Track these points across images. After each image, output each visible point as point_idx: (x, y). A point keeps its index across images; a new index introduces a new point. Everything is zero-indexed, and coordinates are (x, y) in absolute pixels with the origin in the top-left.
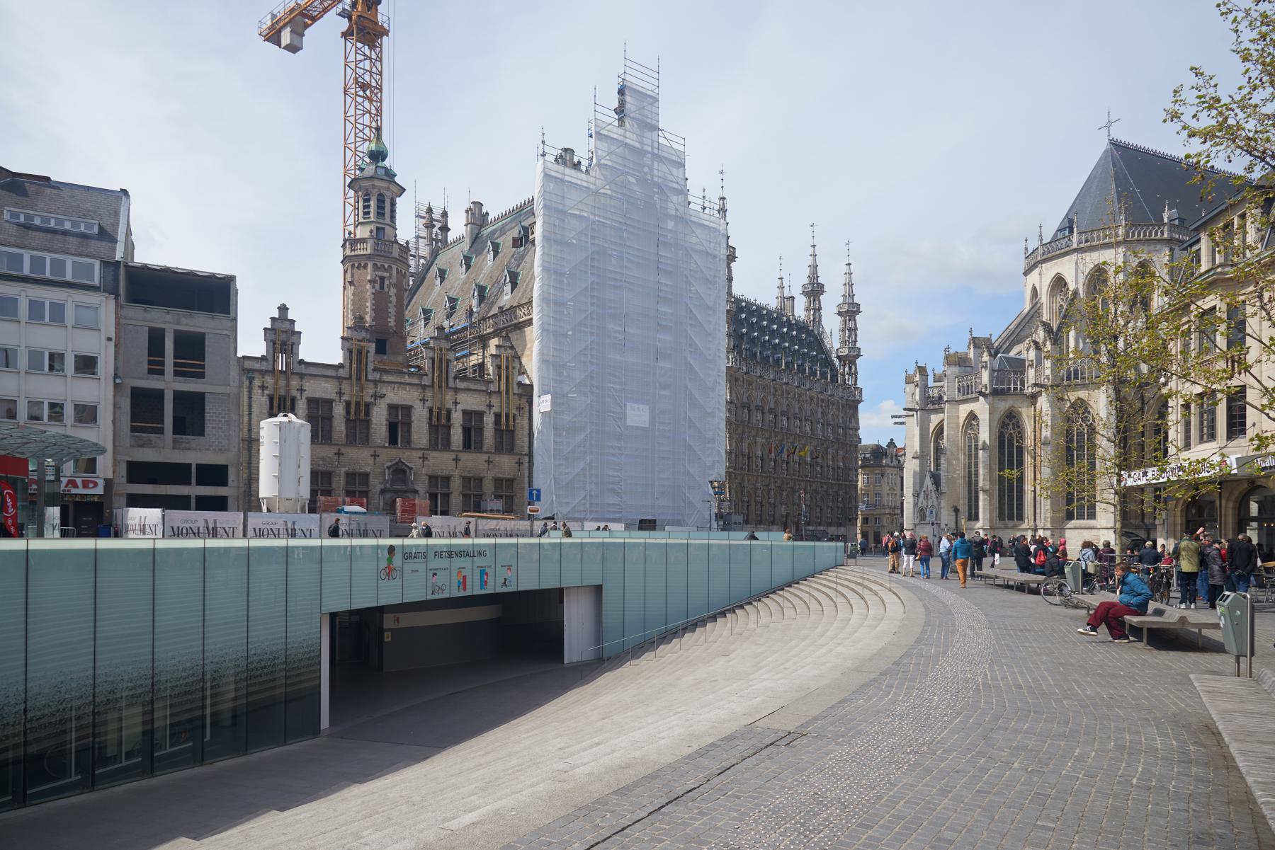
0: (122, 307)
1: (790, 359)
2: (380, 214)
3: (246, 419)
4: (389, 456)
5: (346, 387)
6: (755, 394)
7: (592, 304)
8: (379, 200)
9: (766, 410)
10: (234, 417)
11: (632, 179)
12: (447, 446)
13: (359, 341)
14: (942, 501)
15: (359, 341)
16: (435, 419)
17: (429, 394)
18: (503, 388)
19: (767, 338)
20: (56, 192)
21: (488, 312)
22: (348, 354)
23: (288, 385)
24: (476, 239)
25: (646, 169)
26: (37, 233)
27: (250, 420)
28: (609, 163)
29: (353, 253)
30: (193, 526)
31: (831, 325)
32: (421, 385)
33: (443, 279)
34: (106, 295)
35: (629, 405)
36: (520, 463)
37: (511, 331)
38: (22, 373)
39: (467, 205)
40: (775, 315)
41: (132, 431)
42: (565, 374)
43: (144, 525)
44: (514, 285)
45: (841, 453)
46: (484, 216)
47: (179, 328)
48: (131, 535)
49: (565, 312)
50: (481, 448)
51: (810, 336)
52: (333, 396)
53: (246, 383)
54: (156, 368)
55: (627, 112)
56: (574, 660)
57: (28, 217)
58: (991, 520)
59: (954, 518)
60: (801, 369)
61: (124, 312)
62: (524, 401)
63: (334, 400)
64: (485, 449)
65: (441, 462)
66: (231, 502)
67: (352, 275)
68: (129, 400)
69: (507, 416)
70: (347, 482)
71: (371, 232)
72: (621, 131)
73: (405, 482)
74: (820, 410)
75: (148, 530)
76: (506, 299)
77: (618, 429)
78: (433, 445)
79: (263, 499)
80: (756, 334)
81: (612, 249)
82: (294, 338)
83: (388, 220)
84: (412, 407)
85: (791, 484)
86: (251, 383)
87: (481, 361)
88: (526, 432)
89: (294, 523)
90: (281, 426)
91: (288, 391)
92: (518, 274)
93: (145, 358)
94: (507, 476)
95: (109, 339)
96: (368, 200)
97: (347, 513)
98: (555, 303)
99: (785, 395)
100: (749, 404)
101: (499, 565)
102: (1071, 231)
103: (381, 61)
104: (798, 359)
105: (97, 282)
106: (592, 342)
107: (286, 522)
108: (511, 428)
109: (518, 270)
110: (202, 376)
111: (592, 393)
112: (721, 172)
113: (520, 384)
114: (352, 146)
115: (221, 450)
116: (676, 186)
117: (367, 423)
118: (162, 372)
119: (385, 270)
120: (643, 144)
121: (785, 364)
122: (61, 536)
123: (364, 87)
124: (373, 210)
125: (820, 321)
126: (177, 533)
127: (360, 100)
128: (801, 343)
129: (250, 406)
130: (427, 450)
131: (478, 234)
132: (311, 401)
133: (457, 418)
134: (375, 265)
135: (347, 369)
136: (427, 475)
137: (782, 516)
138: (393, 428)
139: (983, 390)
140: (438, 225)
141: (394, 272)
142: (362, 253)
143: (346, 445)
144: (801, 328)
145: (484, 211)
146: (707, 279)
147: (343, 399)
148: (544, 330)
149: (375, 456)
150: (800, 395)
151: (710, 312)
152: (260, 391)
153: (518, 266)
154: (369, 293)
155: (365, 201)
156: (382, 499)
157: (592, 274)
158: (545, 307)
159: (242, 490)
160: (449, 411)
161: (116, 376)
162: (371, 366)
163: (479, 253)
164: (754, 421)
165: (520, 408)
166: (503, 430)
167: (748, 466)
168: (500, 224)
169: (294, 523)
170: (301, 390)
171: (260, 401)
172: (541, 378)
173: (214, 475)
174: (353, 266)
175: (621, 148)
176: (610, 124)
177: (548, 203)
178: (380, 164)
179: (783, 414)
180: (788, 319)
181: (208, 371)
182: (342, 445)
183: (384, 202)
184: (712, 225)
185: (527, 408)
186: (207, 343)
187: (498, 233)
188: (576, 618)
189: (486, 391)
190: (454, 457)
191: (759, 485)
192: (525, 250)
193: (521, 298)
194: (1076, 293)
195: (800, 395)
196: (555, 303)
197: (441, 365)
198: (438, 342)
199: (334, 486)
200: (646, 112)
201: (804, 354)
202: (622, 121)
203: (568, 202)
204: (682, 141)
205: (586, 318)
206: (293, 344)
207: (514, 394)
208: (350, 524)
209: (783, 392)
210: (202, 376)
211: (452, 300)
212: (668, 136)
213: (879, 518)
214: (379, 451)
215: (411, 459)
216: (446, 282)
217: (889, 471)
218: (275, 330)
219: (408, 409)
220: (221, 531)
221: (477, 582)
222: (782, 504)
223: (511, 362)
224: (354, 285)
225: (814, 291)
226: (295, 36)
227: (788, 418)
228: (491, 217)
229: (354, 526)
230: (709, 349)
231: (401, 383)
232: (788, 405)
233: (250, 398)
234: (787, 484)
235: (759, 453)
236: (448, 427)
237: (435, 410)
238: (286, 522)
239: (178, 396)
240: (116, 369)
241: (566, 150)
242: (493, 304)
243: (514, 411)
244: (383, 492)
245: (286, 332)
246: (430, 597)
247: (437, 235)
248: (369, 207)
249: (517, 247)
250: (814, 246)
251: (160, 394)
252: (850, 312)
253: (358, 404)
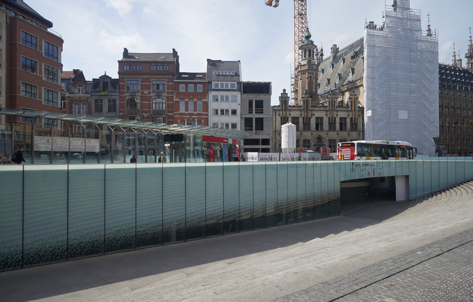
0: (242, 95)
1: (461, 85)
2: (310, 56)
3: (275, 125)
4: (316, 134)
5: (303, 113)
6: (445, 101)
7: (385, 77)
8: (309, 51)
9: (450, 107)
10: (271, 124)
11: (400, 30)
12: (334, 129)
13: (307, 98)
15: (307, 98)
16: (330, 121)
17: (328, 113)
18: (353, 109)
19: (449, 78)
20: (223, 64)
21: (343, 83)
22: (303, 102)
23: (286, 113)
24: (335, 57)
25: (405, 25)
26: (221, 77)
28: (391, 25)
29: (301, 70)
30: (266, 157)
32: (326, 110)
33: (323, 72)
34: (238, 92)
35: (400, 111)
36: (359, 134)
38: (219, 116)
39: (332, 46)
40: (453, 68)
41: (245, 130)
42: (376, 102)
43: (253, 157)
44: (353, 73)
46: (337, 49)
47: (256, 99)
48: (249, 160)
49: (376, 81)
50: (346, 129)
52: (299, 116)
53: (274, 114)
54: (251, 112)
55: (397, 6)
56: (399, 200)
57: (219, 73)
60: (466, 89)
61: (242, 96)
62: (360, 113)
63: (299, 117)
64: (347, 130)
65: (333, 135)
66: (271, 150)
67: (301, 76)
68: (244, 121)
69: (355, 118)
70: (304, 143)
71: (307, 62)
72: (395, 13)
73: (321, 142)
75: (254, 158)
76: (350, 78)
77: (396, 120)
78: (330, 129)
79: (283, 149)
80: (444, 77)
81: (392, 56)
82: (288, 99)
83: (312, 57)
84: (323, 117)
85: (462, 137)
86: (276, 114)
87: (342, 100)
88: (361, 123)
89: (293, 156)
90: (288, 127)
91: (286, 115)
92: (354, 69)
93: (248, 109)
95: (239, 104)
96: (306, 52)
97: (308, 152)
98: (372, 78)
99: (459, 100)
100: (442, 105)
101: (378, 168)
103: (306, 5)
104: (465, 85)
105: (236, 88)
106: (385, 90)
107: (291, 156)
108: (356, 122)
109: (354, 67)
110: (262, 113)
111: (386, 108)
112: (428, 15)
113: (359, 107)
114: (297, 34)
115: (268, 134)
116: (417, 28)
117: (309, 123)
118: (252, 113)
120: (403, 16)
121: (459, 87)
122: (131, 162)
123: (301, 15)
124: (307, 55)
126: (262, 159)
127: (300, 19)
128: (465, 78)
129: (276, 121)
130: (328, 131)
131: (335, 56)
132: (292, 118)
133: (338, 120)
135: (303, 107)
136: (328, 139)
137: (458, 150)
138: (317, 125)
140: (320, 54)
141: (314, 74)
142: (304, 69)
143: (303, 131)
144: (465, 72)
145: (337, 47)
146: (431, 61)
147: (302, 116)
148: (368, 88)
149: (312, 134)
150: (466, 100)
151: (432, 74)
152: (278, 116)
153: (354, 66)
154: (307, 82)
155: (305, 52)
156: (314, 147)
157: (385, 66)
158: (368, 80)
159: (274, 146)
160: (335, 118)
161: (241, 115)
162: (310, 105)
163: (337, 62)
164: (445, 112)
165: (359, 115)
166: (353, 123)
167: (442, 130)
168: (344, 51)
169: (293, 156)
170: (290, 115)
171: (278, 119)
172: (367, 105)
173: (266, 142)
174: (301, 74)
175: (395, 19)
176: (391, 11)
177: (369, 44)
178: (309, 40)
179: (458, 108)
180: (459, 69)
181: (264, 111)
182: (302, 131)
183: (310, 52)
184: (432, 40)
185: (361, 115)
186: (264, 103)
187: (344, 54)
188: (400, 186)
189: (347, 111)
190: (337, 133)
191: (447, 138)
192: (356, 60)
193: (356, 77)
195: (466, 100)
196: (372, 78)
197: (332, 103)
198: (331, 96)
199: (300, 144)
200: (404, 4)
201: (467, 82)
202: (395, 10)
203: (376, 42)
204: (419, 11)
205: (383, 82)
206: (287, 101)
207: (357, 111)
208: (309, 156)
210: (262, 113)
211: (329, 80)
212: (414, 11)
214: (313, 132)
215: (323, 134)
216: (325, 73)
218: (282, 97)
219: (322, 118)
220: (273, 159)
221: (372, 175)
222: (458, 145)
223: (354, 100)
224: (302, 80)
226: (277, 2)
227: (460, 110)
228: (339, 50)
229: (310, 157)
230: (432, 88)
231: (319, 110)
232: (454, 104)
233: (276, 118)
234: (460, 137)
235: (447, 125)
236: (335, 123)
237: (331, 118)
238: (291, 156)
239: (256, 119)
240: (241, 112)
241: (371, 22)
242: (345, 80)
243: (357, 117)
244: (314, 145)
245: (285, 97)
246: (361, 178)
247: (319, 57)
248: (306, 54)
249: (353, 59)
250: (471, 37)
251: (252, 119)
253: (307, 118)
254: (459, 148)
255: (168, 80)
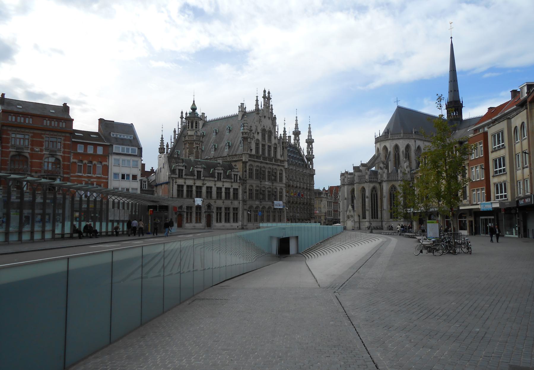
14: (355, 213)
27: (173, 192)
31: (303, 145)
32: (214, 180)
37: (232, 162)
45: (308, 193)
51: (295, 149)
58: (370, 219)
59: (358, 218)
74: (302, 178)
86: (173, 181)
94: (236, 207)
102: (388, 134)
119: (198, 144)
125: (299, 145)
134: (196, 143)
139: (367, 181)
147: (195, 185)
156: (205, 214)
194: (390, 152)
209: (290, 172)
213: (320, 217)
215: (212, 202)
217: (323, 199)
225: (297, 133)
231: (209, 180)
233: (173, 186)
244: (205, 212)
252: (310, 142)
254: (291, 214)
255: (64, 138)
